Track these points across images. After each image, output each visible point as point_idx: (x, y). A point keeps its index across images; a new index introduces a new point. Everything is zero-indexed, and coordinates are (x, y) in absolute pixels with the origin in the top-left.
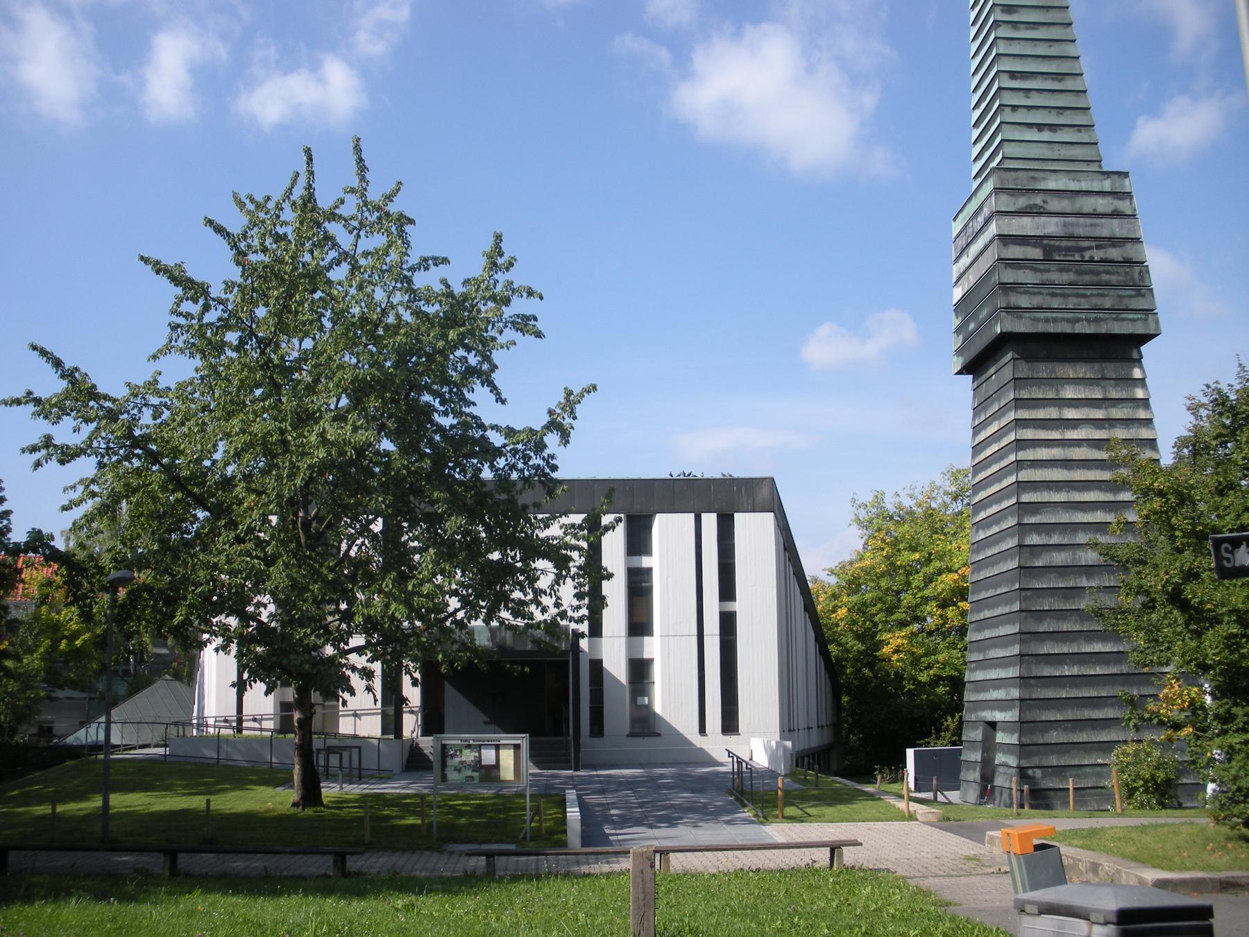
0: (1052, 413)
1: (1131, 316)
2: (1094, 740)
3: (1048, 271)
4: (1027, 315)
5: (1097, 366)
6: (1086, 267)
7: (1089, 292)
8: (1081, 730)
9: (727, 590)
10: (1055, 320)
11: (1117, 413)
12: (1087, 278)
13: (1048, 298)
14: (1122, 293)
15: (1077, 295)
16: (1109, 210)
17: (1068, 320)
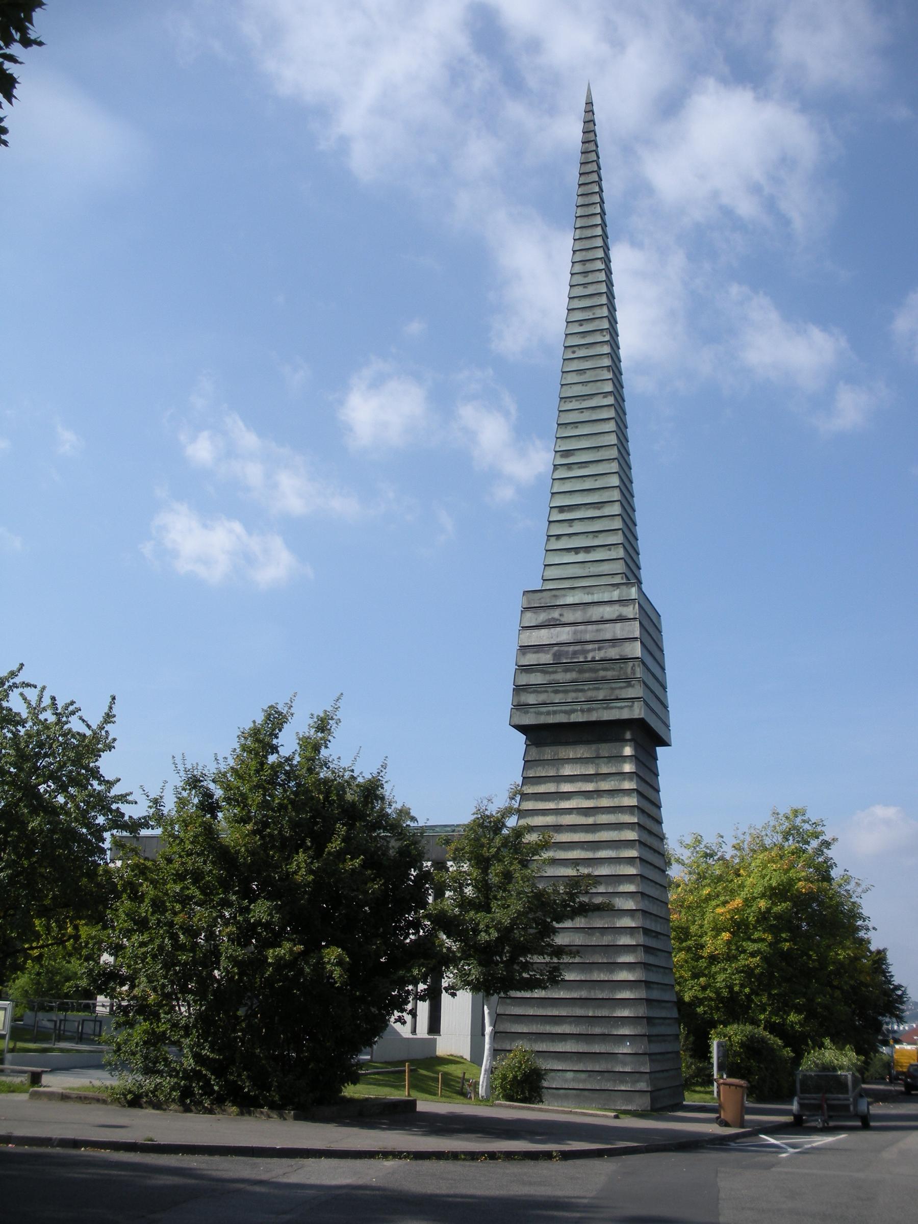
0: (551, 788)
1: (619, 705)
2: (552, 1050)
3: (555, 672)
4: (532, 710)
5: (594, 747)
6: (587, 666)
7: (586, 687)
8: (542, 1041)
10: (555, 712)
11: (605, 785)
12: (587, 675)
13: (552, 695)
14: (614, 685)
16: (614, 616)
17: (565, 712)
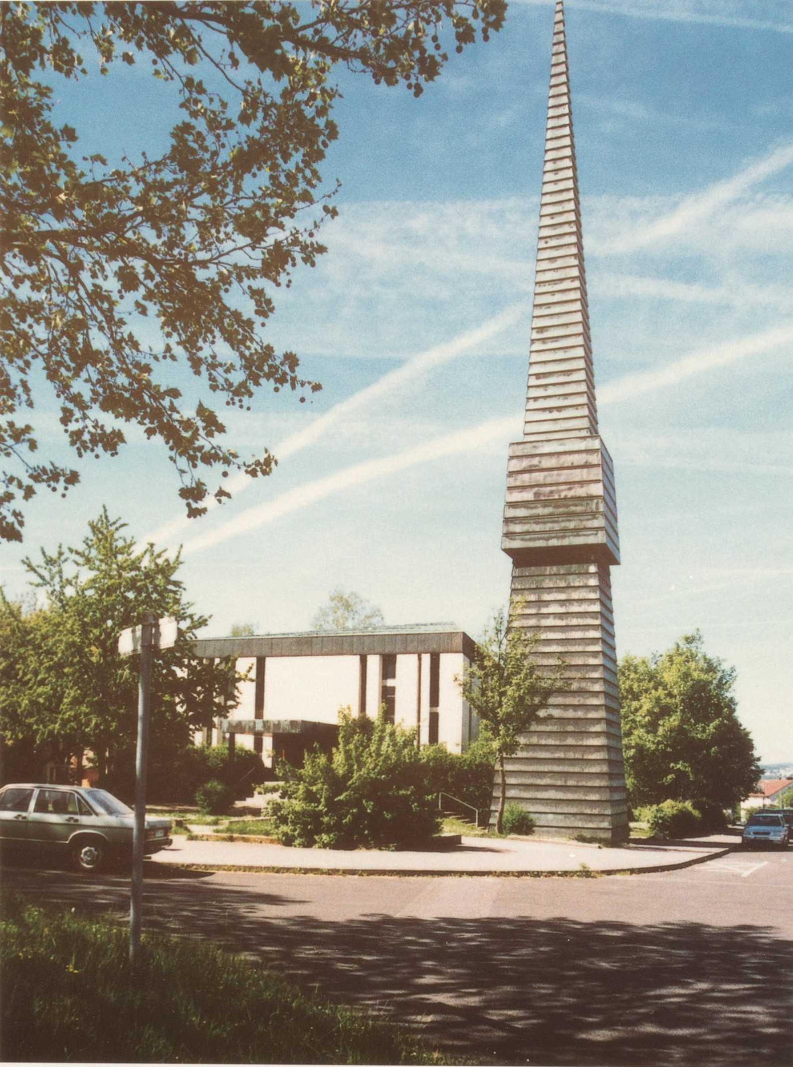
3: (535, 508)
9: (434, 700)
12: (561, 510)
15: (551, 522)
16: (582, 463)
